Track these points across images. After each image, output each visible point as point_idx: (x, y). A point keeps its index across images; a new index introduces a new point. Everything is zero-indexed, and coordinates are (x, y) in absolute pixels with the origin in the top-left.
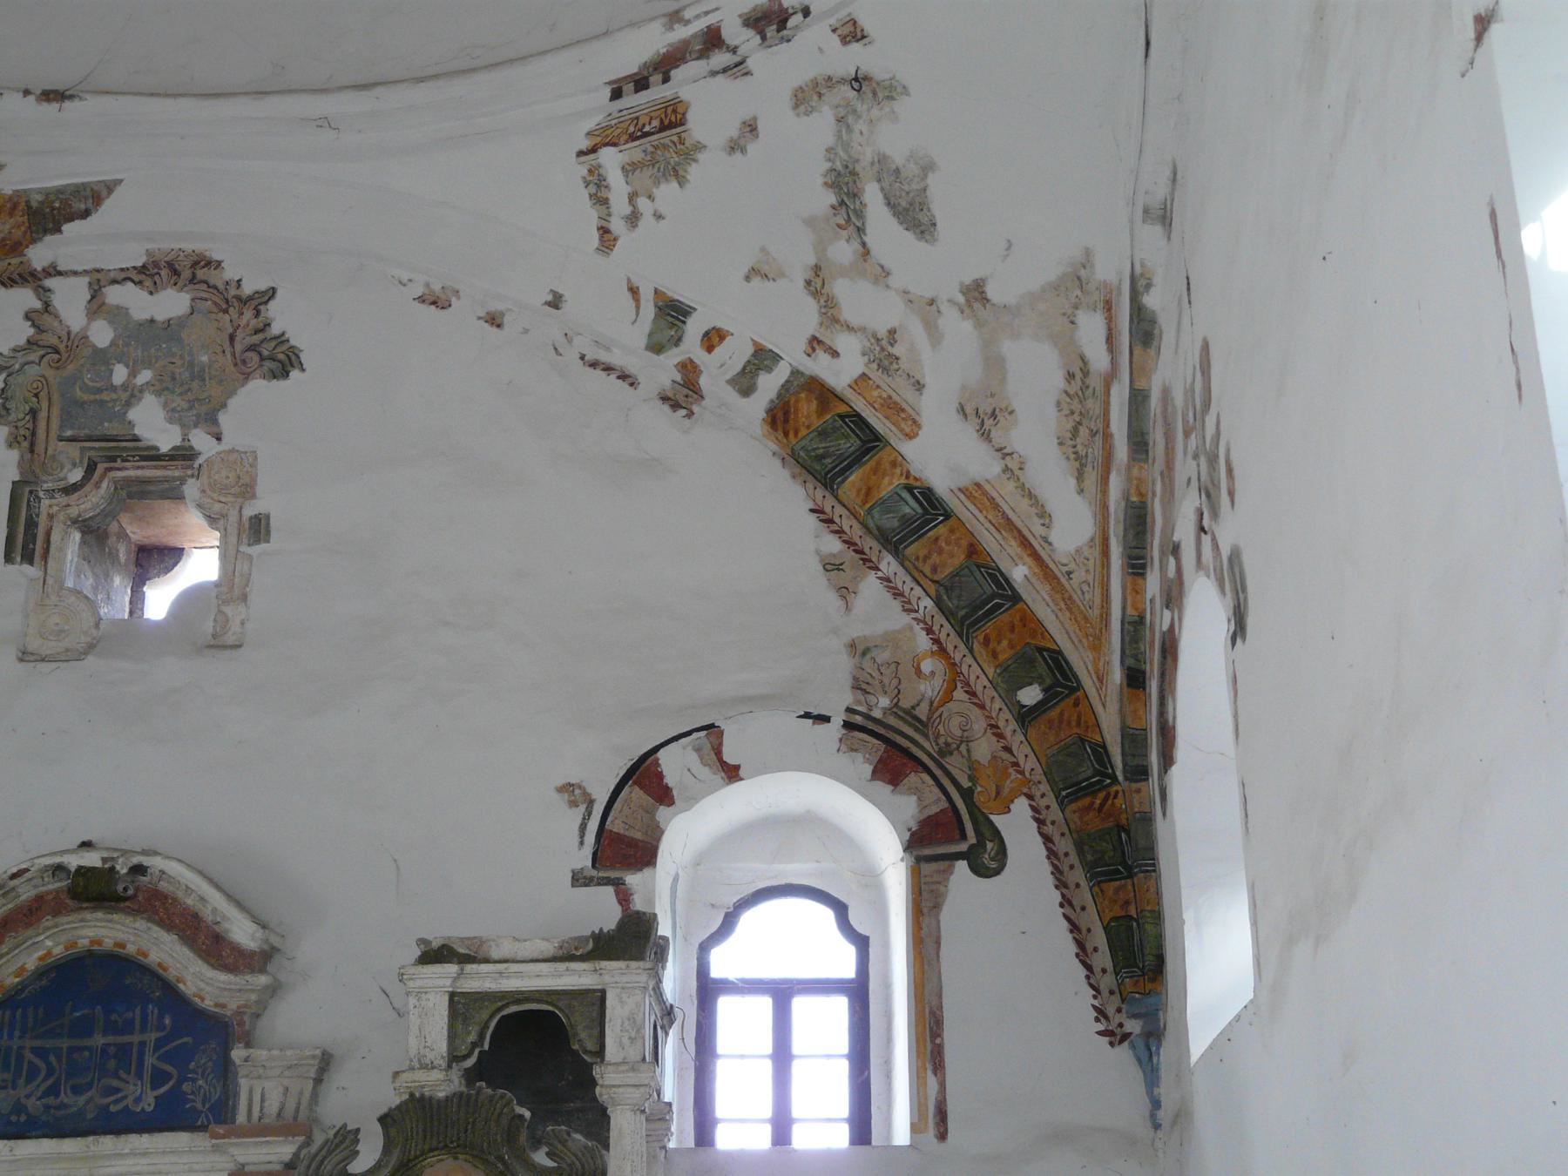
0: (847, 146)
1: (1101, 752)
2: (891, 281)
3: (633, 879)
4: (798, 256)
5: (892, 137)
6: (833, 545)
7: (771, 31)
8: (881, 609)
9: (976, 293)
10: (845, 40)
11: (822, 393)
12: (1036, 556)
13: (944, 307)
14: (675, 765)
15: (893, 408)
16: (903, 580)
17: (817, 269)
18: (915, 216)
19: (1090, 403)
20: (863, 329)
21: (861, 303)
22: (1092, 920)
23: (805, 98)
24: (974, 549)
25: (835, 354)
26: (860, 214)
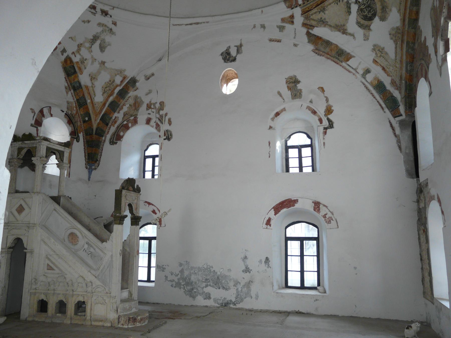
0: (100, 34)
1: (92, 130)
2: (92, 53)
3: (39, 128)
4: (80, 40)
5: (108, 38)
6: (66, 85)
7: (104, 14)
8: (70, 97)
9: (103, 63)
10: (113, 23)
11: (71, 61)
12: (92, 99)
13: (97, 61)
14: (46, 111)
15: (80, 69)
16: (73, 94)
17: (81, 44)
18: (102, 48)
19: (111, 86)
20: (82, 56)
21: (84, 52)
22: (86, 151)
23: (99, 24)
24: (83, 95)
25: (75, 56)
26: (94, 43)
